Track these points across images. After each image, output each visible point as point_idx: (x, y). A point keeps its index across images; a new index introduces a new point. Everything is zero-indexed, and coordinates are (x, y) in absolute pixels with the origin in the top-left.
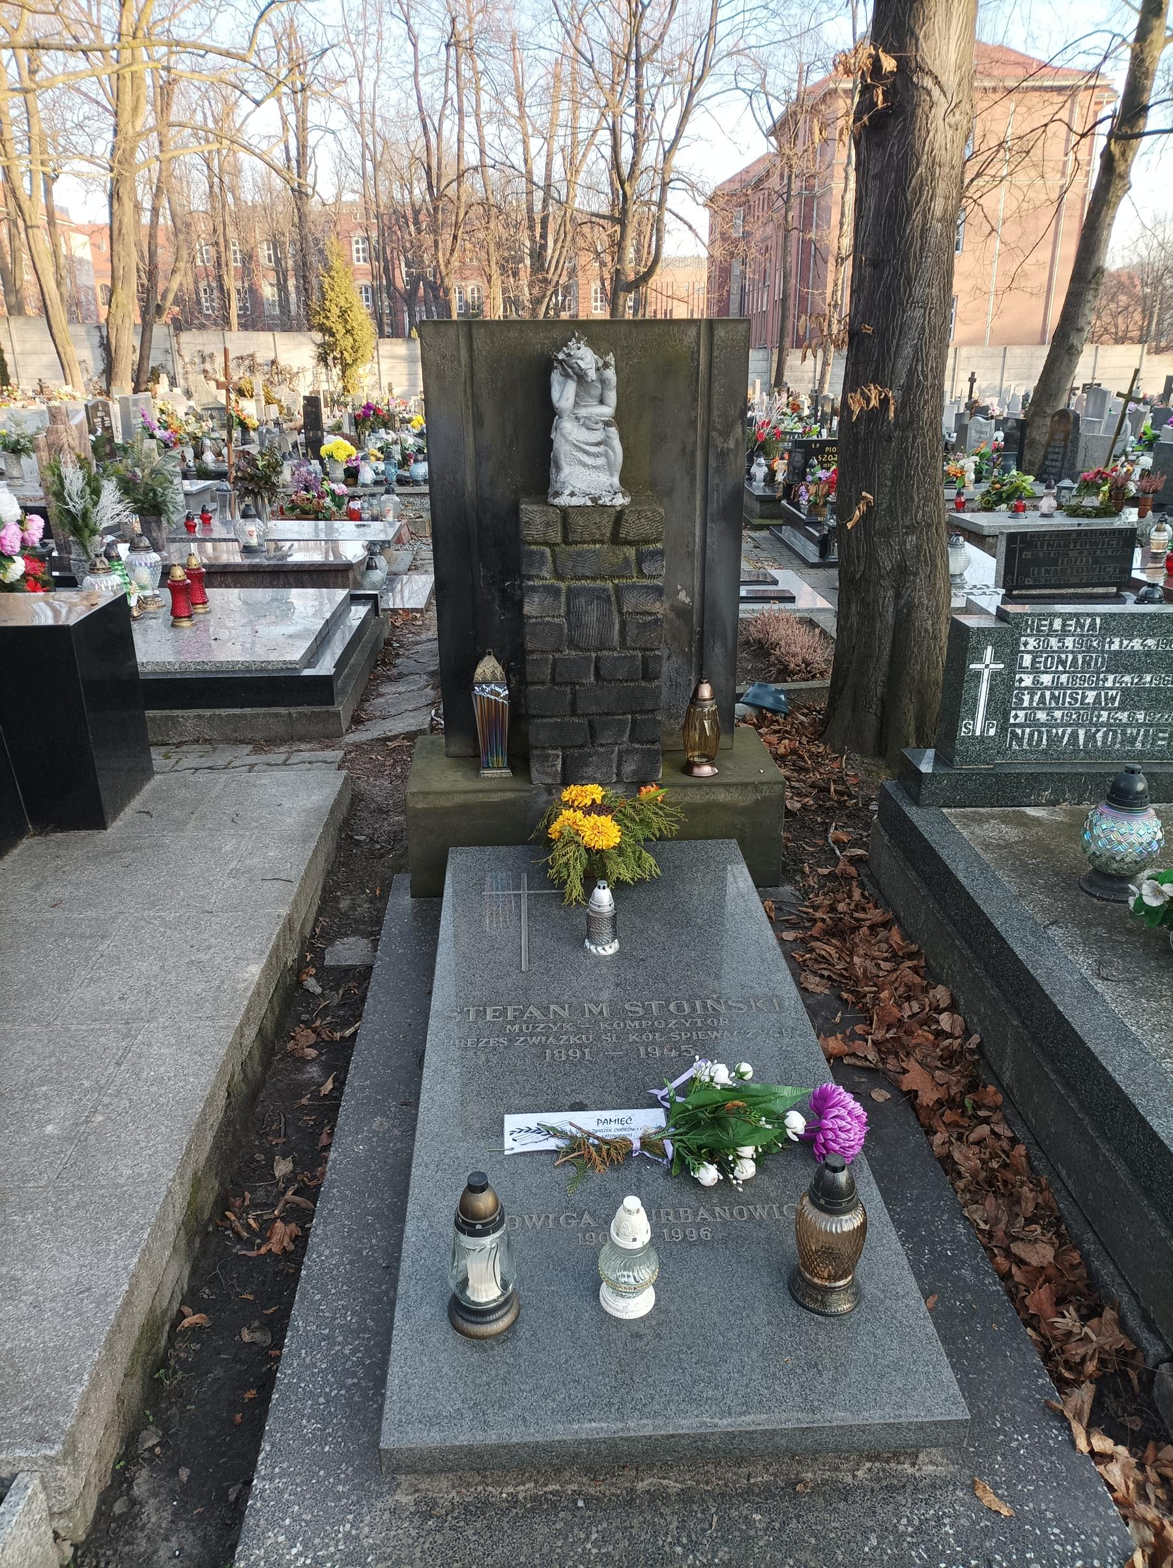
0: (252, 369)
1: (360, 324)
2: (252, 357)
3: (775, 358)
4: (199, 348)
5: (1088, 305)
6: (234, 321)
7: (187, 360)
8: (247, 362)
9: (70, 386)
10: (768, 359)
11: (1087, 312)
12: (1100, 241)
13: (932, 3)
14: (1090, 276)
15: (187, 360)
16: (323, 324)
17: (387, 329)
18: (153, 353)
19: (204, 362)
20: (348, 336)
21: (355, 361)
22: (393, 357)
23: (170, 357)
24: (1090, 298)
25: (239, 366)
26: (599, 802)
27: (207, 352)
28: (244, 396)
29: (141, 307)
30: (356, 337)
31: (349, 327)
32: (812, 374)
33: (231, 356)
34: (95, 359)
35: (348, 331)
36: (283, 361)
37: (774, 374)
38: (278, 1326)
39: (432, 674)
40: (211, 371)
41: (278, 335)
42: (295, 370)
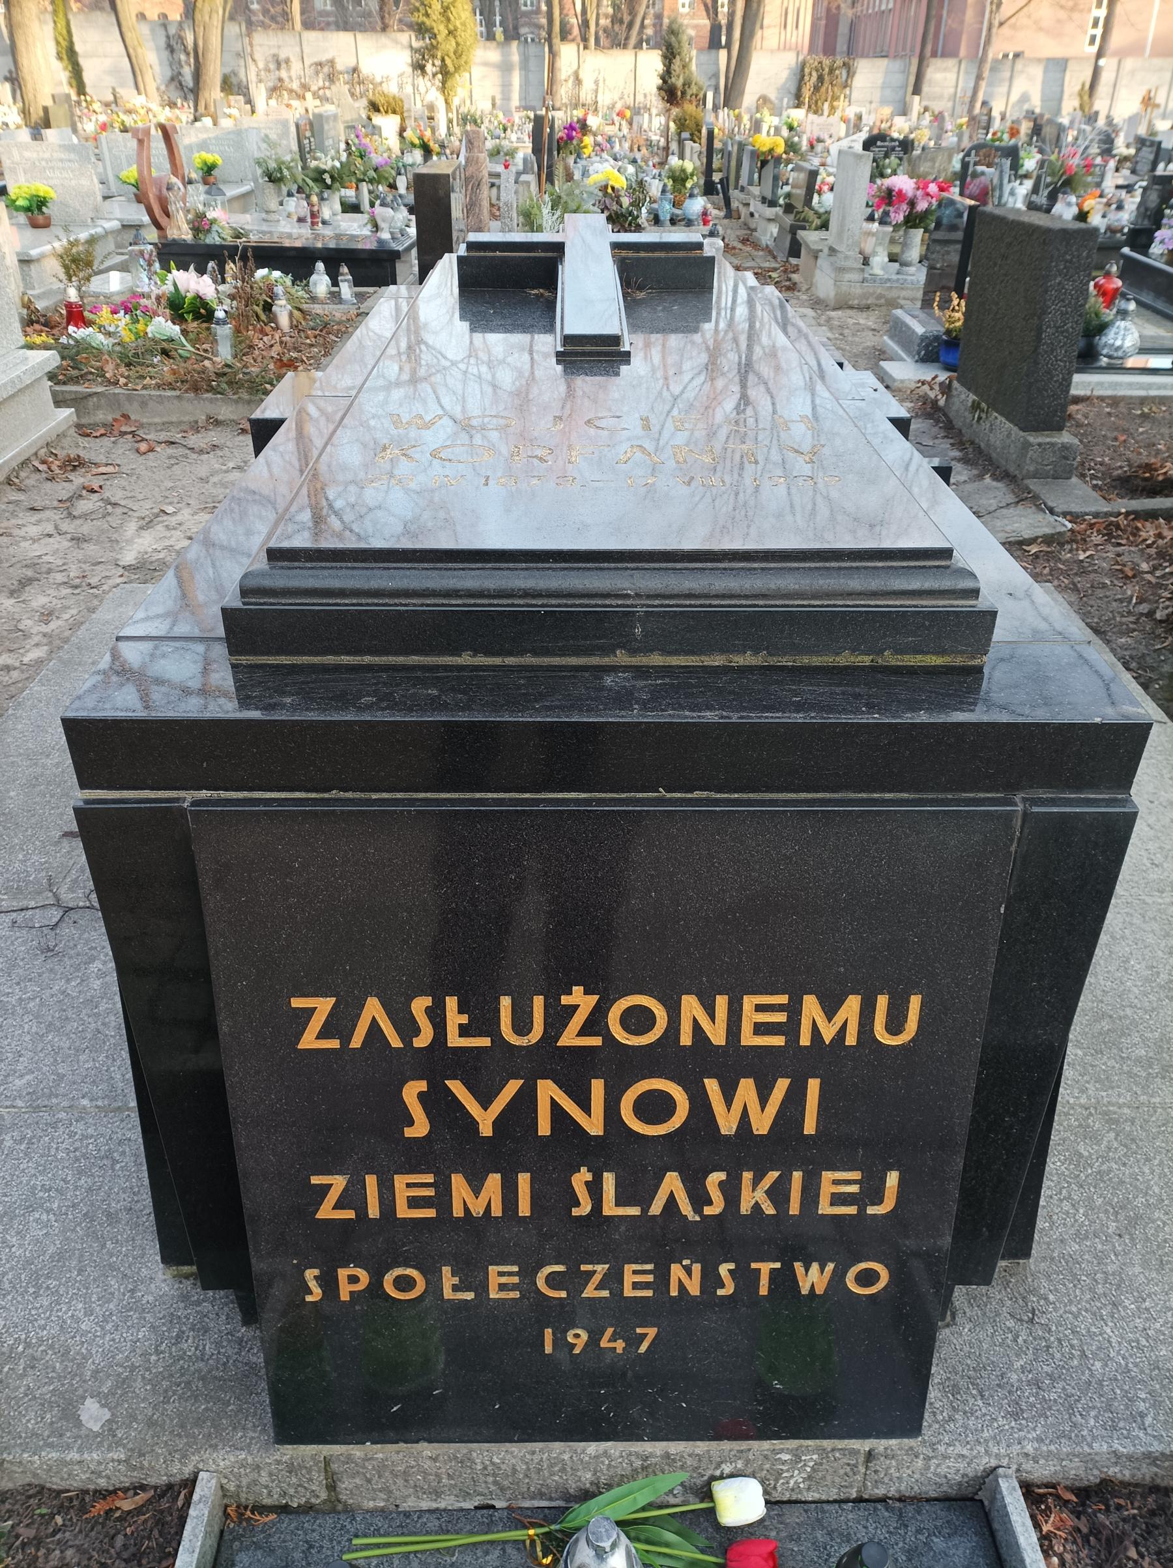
0: (331, 78)
1: (463, 24)
2: (332, 62)
3: (914, 69)
7: (261, 65)
8: (326, 69)
9: (143, 96)
16: (423, 23)
17: (498, 31)
19: (279, 67)
20: (451, 38)
21: (457, 69)
22: (486, 64)
25: (317, 73)
27: (282, 56)
28: (378, 110)
30: (460, 40)
31: (451, 27)
32: (952, 90)
33: (307, 62)
34: (161, 64)
35: (450, 32)
36: (365, 70)
39: (472, 330)
40: (287, 80)
41: (359, 36)
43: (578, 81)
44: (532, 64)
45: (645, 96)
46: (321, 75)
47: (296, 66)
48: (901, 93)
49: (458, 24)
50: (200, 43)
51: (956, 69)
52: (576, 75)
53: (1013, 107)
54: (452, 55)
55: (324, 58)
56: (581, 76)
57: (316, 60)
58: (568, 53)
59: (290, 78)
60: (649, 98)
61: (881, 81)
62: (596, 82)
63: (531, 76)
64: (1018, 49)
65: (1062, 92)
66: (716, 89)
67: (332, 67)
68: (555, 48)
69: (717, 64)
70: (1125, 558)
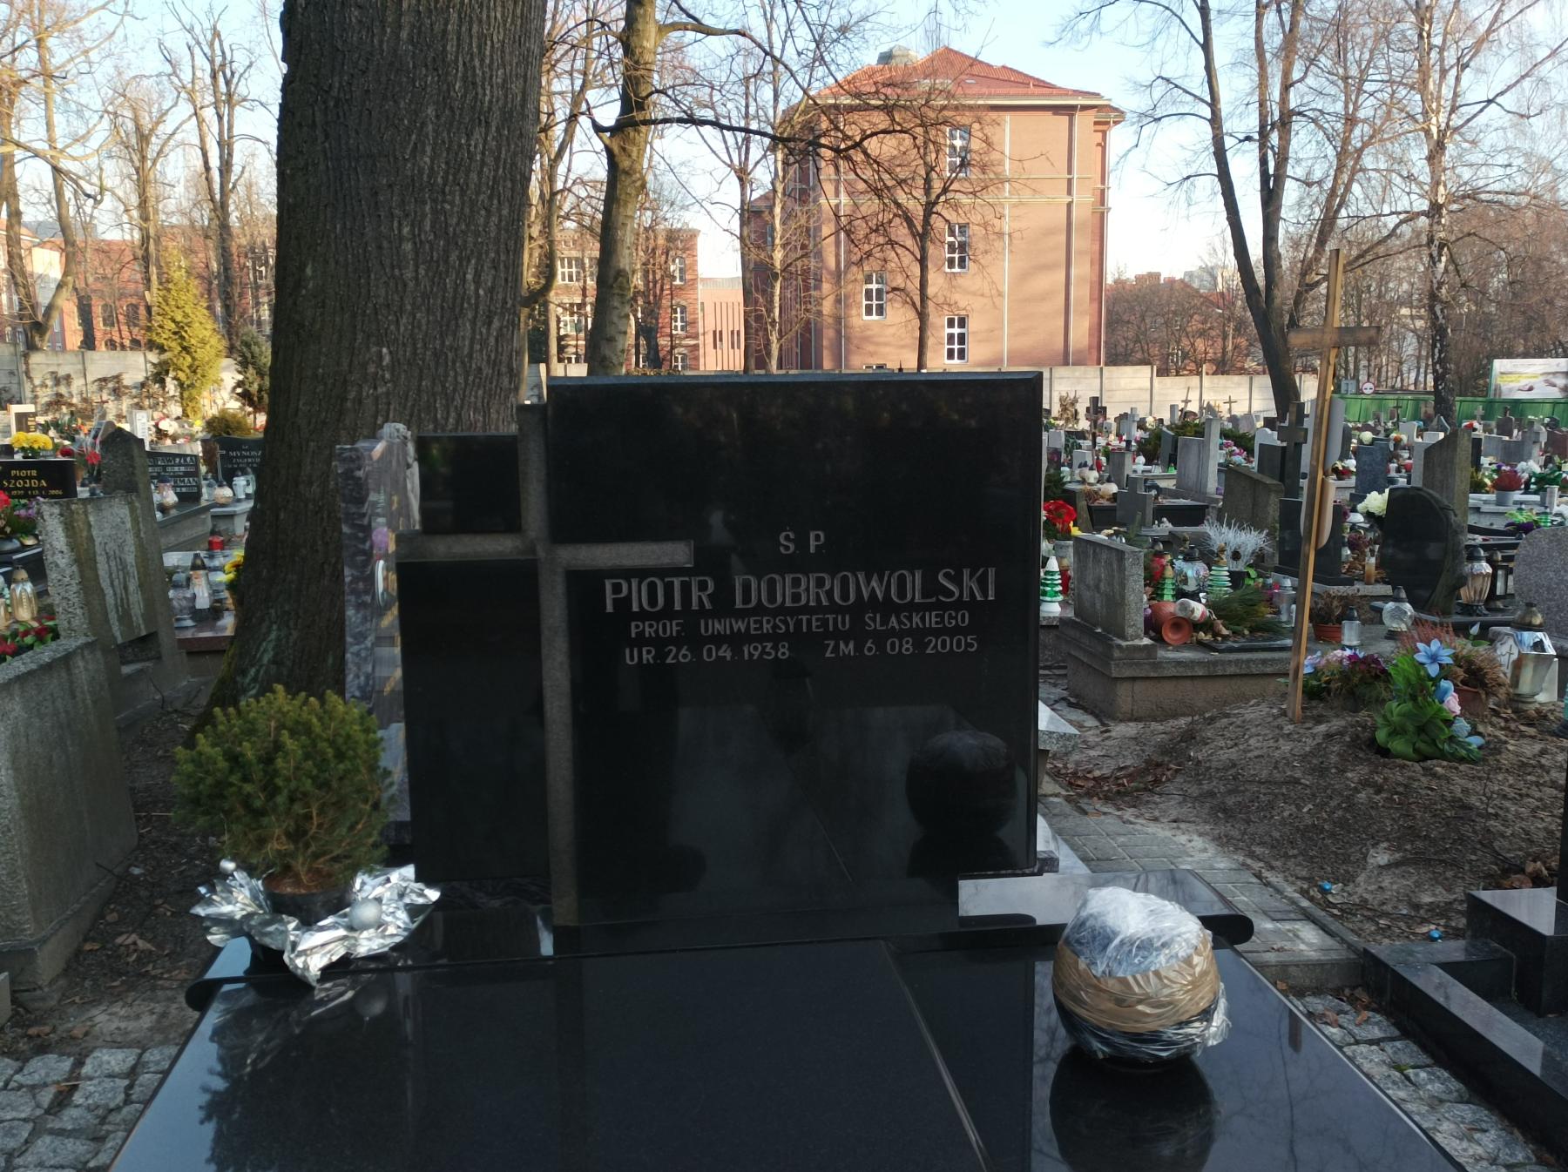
2: (117, 378)
4: (51, 369)
5: (616, 312)
8: (111, 385)
11: (615, 319)
12: (615, 242)
13: (550, 5)
14: (611, 280)
15: (37, 382)
23: (15, 380)
24: (616, 304)
26: (332, 697)
29: (1162, 894)
33: (90, 378)
38: (1526, 355)
47: (77, 383)
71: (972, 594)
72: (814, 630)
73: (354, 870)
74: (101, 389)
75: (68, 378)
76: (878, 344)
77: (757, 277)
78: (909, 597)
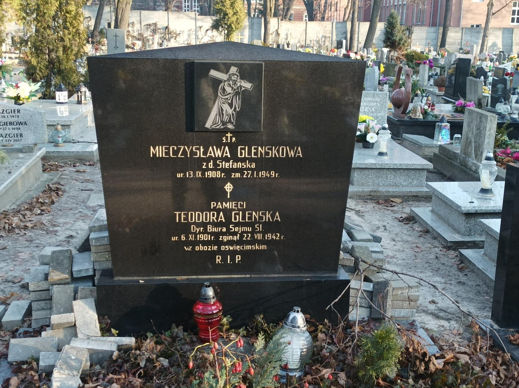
0: (154, 31)
1: (240, 10)
2: (155, 24)
6: (272, 16)
8: (152, 27)
10: (437, 32)
18: (102, 21)
32: (460, 41)
33: (143, 24)
36: (172, 28)
37: (440, 40)
42: (178, 32)
43: (278, 34)
44: (255, 27)
45: (311, 41)
46: (149, 30)
47: (137, 26)
48: (435, 42)
49: (238, 10)
50: (120, 17)
51: (461, 32)
52: (277, 31)
53: (489, 48)
54: (235, 23)
55: (151, 22)
56: (279, 32)
57: (147, 23)
58: (273, 22)
59: (134, 31)
60: (312, 42)
61: (425, 36)
62: (287, 35)
63: (254, 32)
64: (478, 23)
65: (512, 42)
66: (346, 38)
67: (155, 26)
68: (268, 20)
69: (346, 27)
70: (34, 253)
71: (275, 154)
72: (182, 221)
73: (42, 331)
74: (147, 29)
75: (133, 23)
76: (474, 14)
77: (454, 165)
78: (193, 221)
